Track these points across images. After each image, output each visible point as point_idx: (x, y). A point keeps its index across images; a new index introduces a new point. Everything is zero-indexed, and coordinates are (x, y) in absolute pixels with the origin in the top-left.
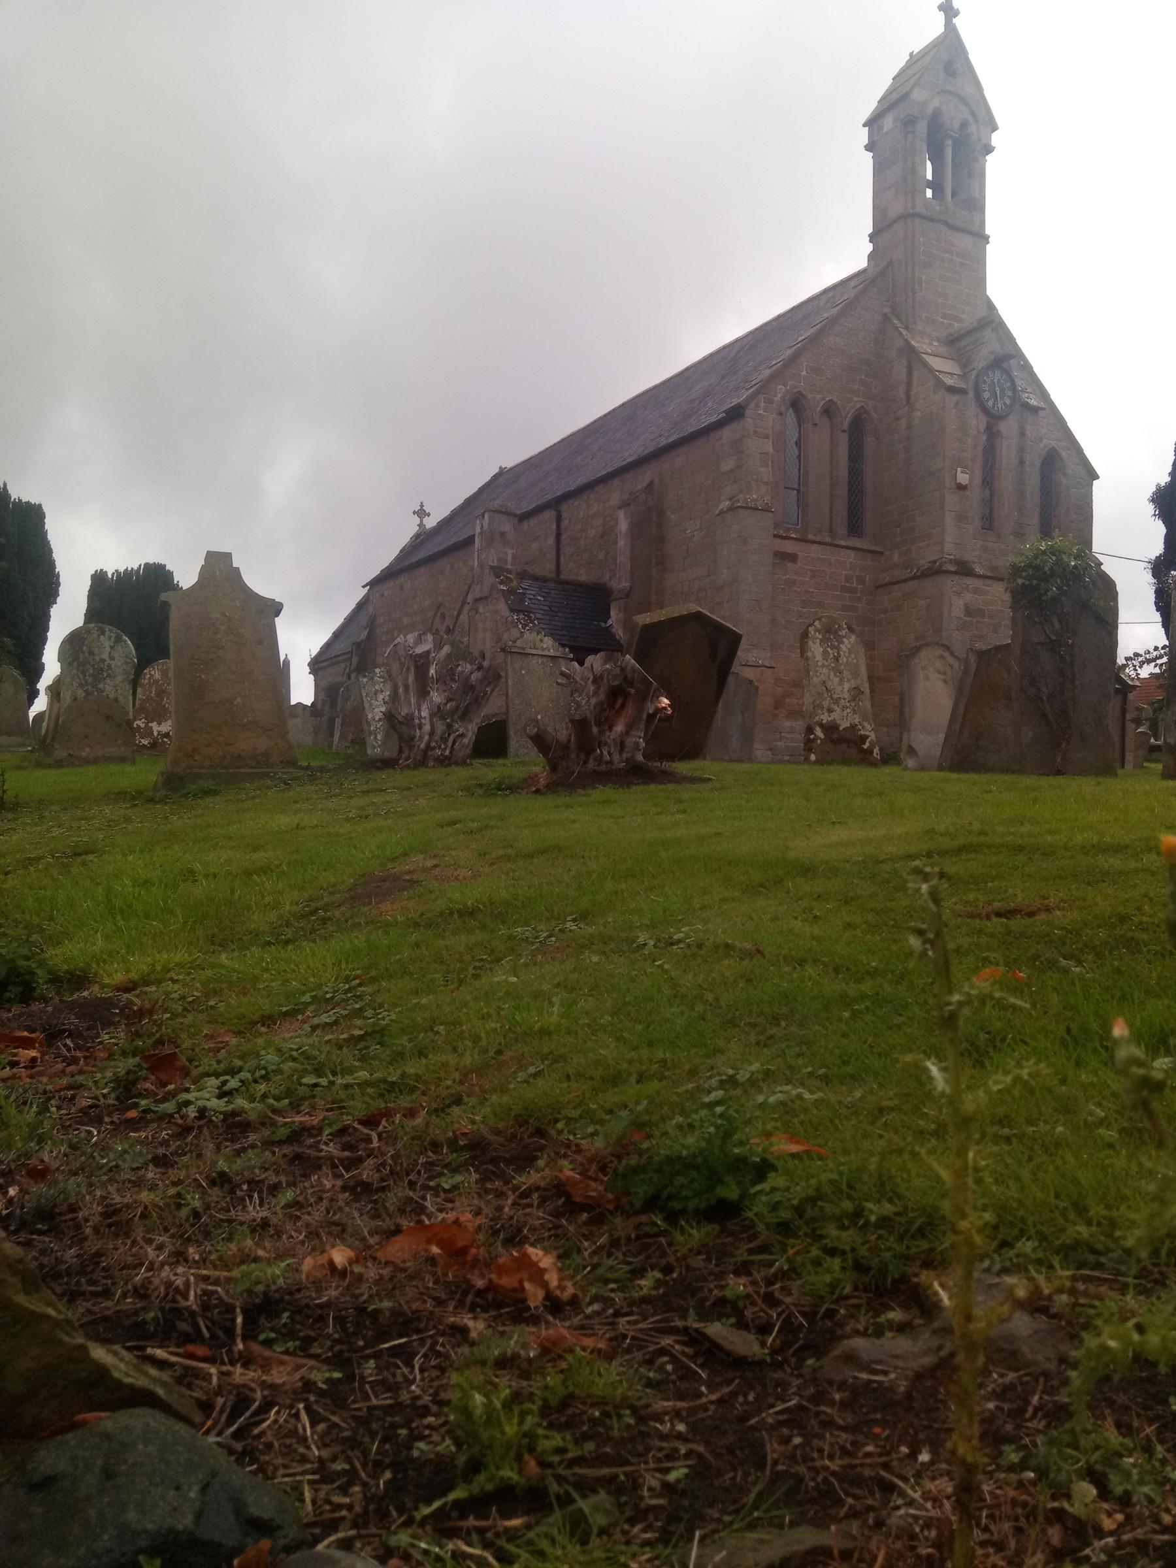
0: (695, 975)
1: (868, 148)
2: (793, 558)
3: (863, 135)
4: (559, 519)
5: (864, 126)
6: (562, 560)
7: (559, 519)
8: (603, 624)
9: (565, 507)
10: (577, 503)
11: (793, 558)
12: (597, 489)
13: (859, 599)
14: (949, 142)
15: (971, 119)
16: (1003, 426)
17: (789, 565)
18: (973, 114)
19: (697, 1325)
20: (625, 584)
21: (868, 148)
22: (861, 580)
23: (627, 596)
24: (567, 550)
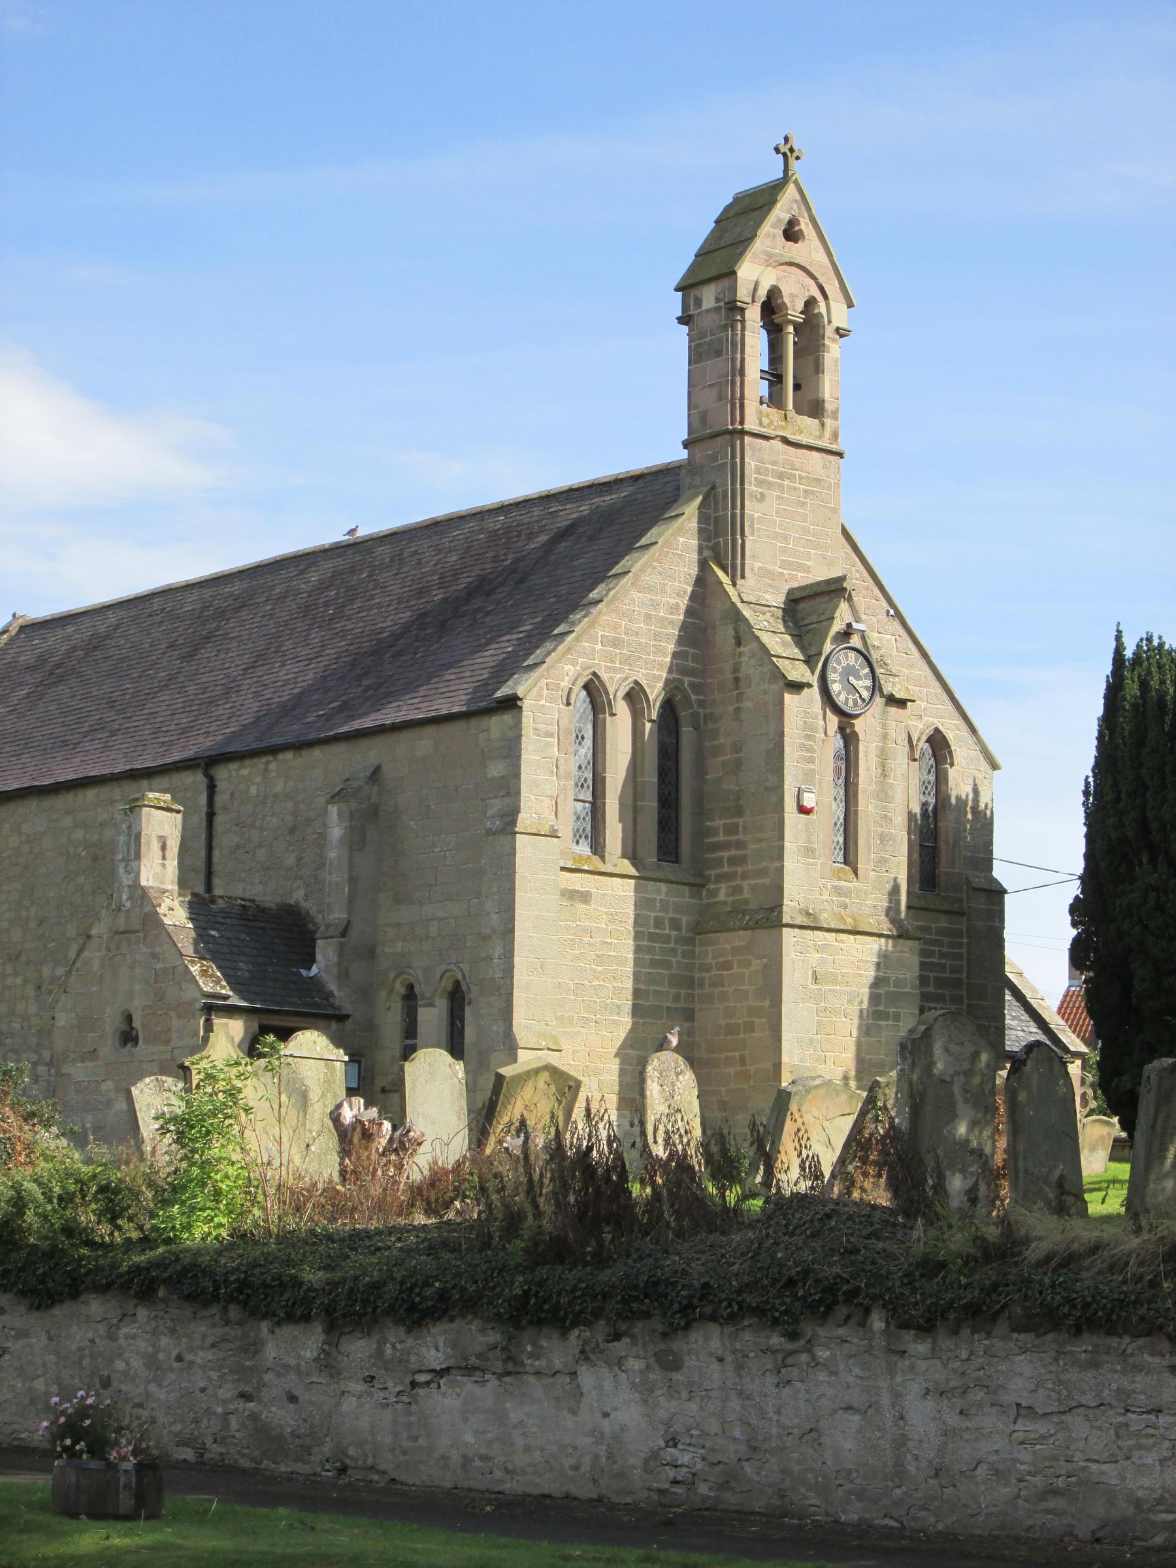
0: (799, 1249)
1: (682, 320)
2: (585, 897)
3: (675, 303)
4: (212, 788)
5: (677, 290)
6: (216, 854)
7: (212, 788)
8: (304, 972)
9: (225, 774)
10: (245, 772)
11: (585, 897)
12: (280, 756)
13: (673, 951)
14: (791, 329)
15: (819, 297)
16: (859, 725)
17: (581, 906)
18: (821, 289)
19: (757, 1004)
20: (338, 915)
21: (682, 320)
22: (675, 924)
23: (344, 934)
24: (225, 840)
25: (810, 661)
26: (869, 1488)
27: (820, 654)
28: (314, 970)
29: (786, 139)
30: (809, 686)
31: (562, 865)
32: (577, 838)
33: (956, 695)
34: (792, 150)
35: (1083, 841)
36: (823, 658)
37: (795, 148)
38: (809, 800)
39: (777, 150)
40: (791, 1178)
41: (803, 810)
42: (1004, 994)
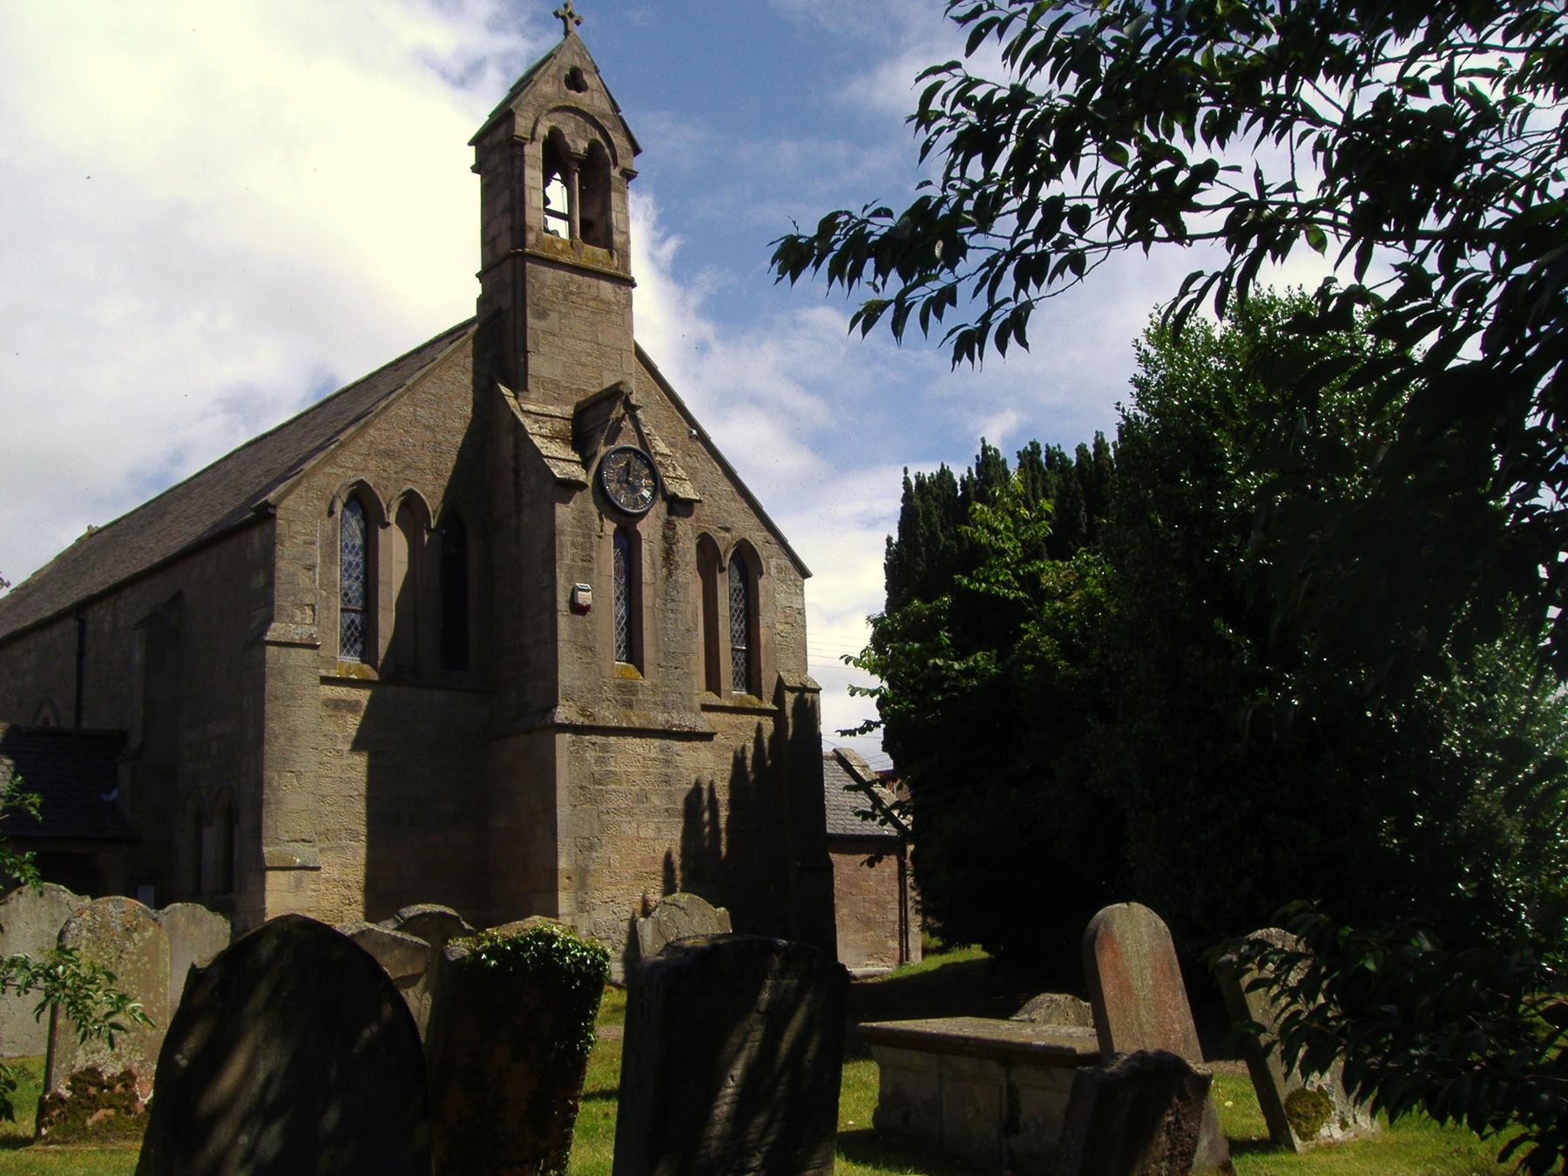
1: (475, 169)
21: (475, 169)
25: (585, 464)
26: (934, 192)
27: (595, 454)
28: (115, 794)
29: (566, 6)
30: (759, 724)
31: (323, 673)
32: (346, 644)
33: (740, 475)
34: (571, 15)
35: (883, 572)
36: (597, 461)
37: (576, 13)
38: (584, 598)
39: (556, 14)
40: (885, 685)
41: (578, 609)
42: (439, 1011)
